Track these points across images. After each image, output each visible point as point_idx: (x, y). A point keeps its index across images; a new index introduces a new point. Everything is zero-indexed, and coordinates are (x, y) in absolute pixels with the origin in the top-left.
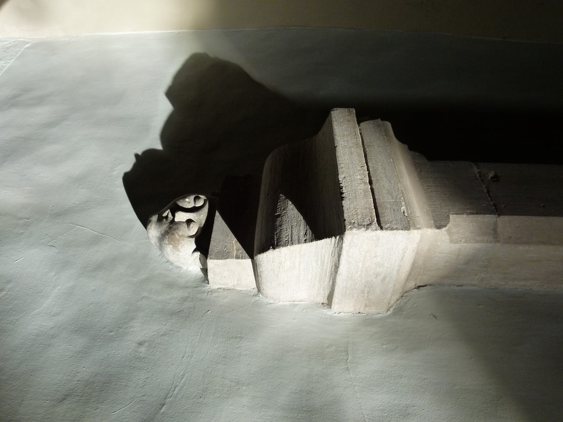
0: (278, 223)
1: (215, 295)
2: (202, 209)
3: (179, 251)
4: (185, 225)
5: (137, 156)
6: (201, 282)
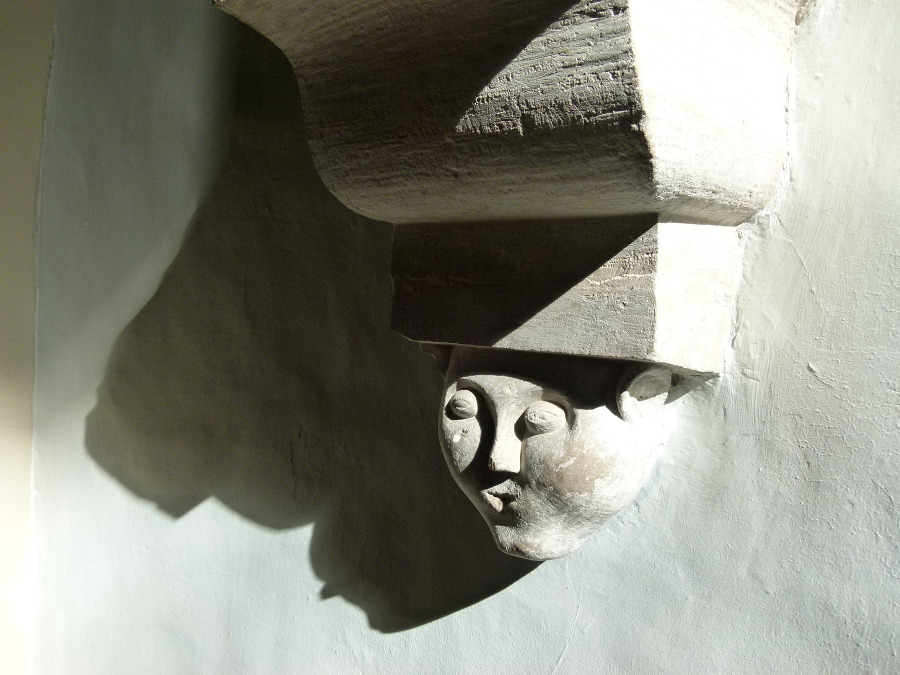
0: (551, 120)
1: (755, 355)
2: (487, 392)
4: (535, 442)
5: (326, 594)
6: (710, 400)
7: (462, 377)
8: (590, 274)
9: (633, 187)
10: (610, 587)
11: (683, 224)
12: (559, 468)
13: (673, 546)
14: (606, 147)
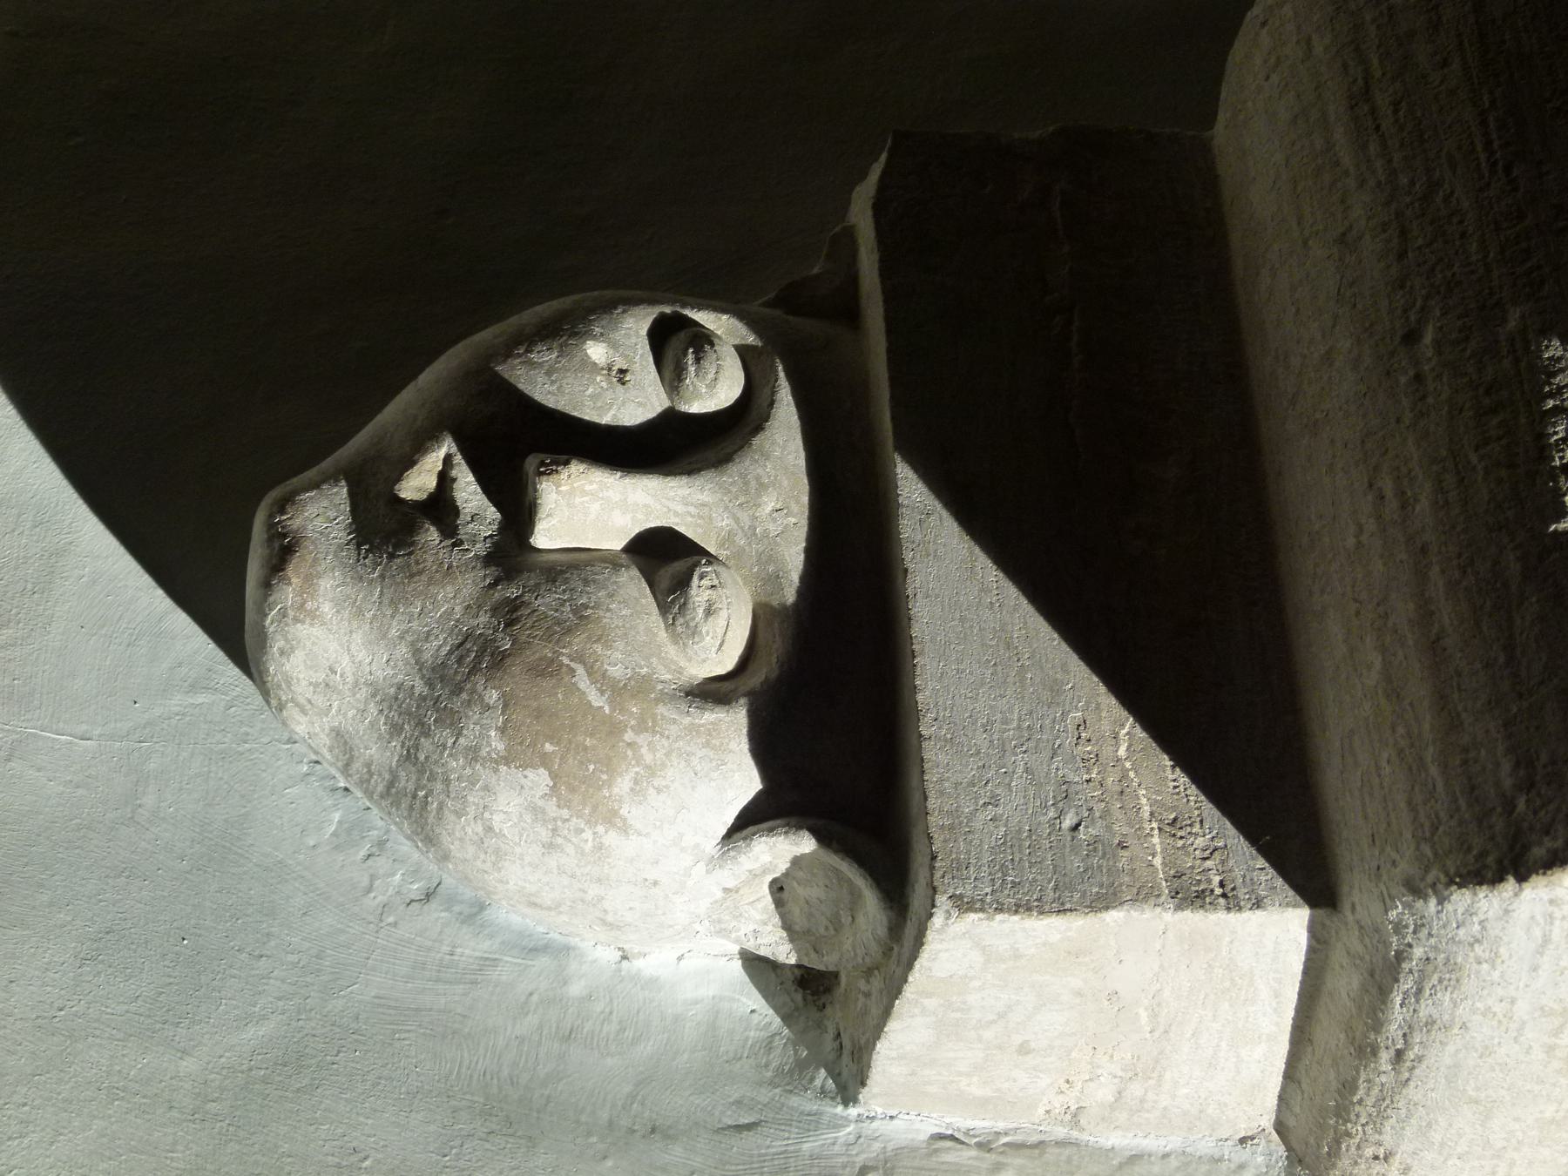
2: (756, 441)
3: (611, 818)
6: (772, 1084)
9: (1428, 834)
11: (1299, 978)
12: (573, 665)
13: (330, 1007)
14: (1538, 759)
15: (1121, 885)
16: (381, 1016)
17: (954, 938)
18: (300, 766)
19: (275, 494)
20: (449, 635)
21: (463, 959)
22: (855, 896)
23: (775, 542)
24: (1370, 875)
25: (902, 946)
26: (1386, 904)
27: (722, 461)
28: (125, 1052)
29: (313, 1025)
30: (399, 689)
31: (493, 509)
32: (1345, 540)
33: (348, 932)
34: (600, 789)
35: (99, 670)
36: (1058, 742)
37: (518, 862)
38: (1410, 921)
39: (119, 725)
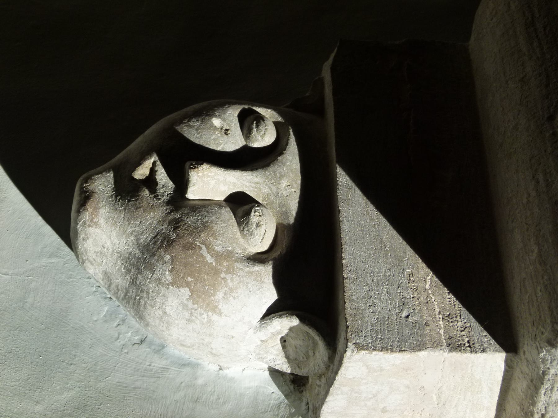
2: (280, 158)
3: (214, 309)
7: (292, 128)
8: (438, 276)
10: (36, 312)
11: (500, 383)
12: (201, 245)
15: (426, 341)
16: (120, 390)
17: (355, 361)
18: (92, 288)
19: (84, 176)
20: (151, 232)
21: (155, 368)
22: (315, 344)
23: (287, 199)
24: (532, 338)
25: (334, 365)
26: (539, 350)
27: (265, 166)
28: (13, 402)
29: (91, 393)
30: (130, 254)
31: (172, 183)
32: (522, 200)
33: (108, 356)
34: (210, 297)
35: (13, 247)
36: (401, 281)
37: (176, 327)
38: (549, 358)
39: (20, 270)
